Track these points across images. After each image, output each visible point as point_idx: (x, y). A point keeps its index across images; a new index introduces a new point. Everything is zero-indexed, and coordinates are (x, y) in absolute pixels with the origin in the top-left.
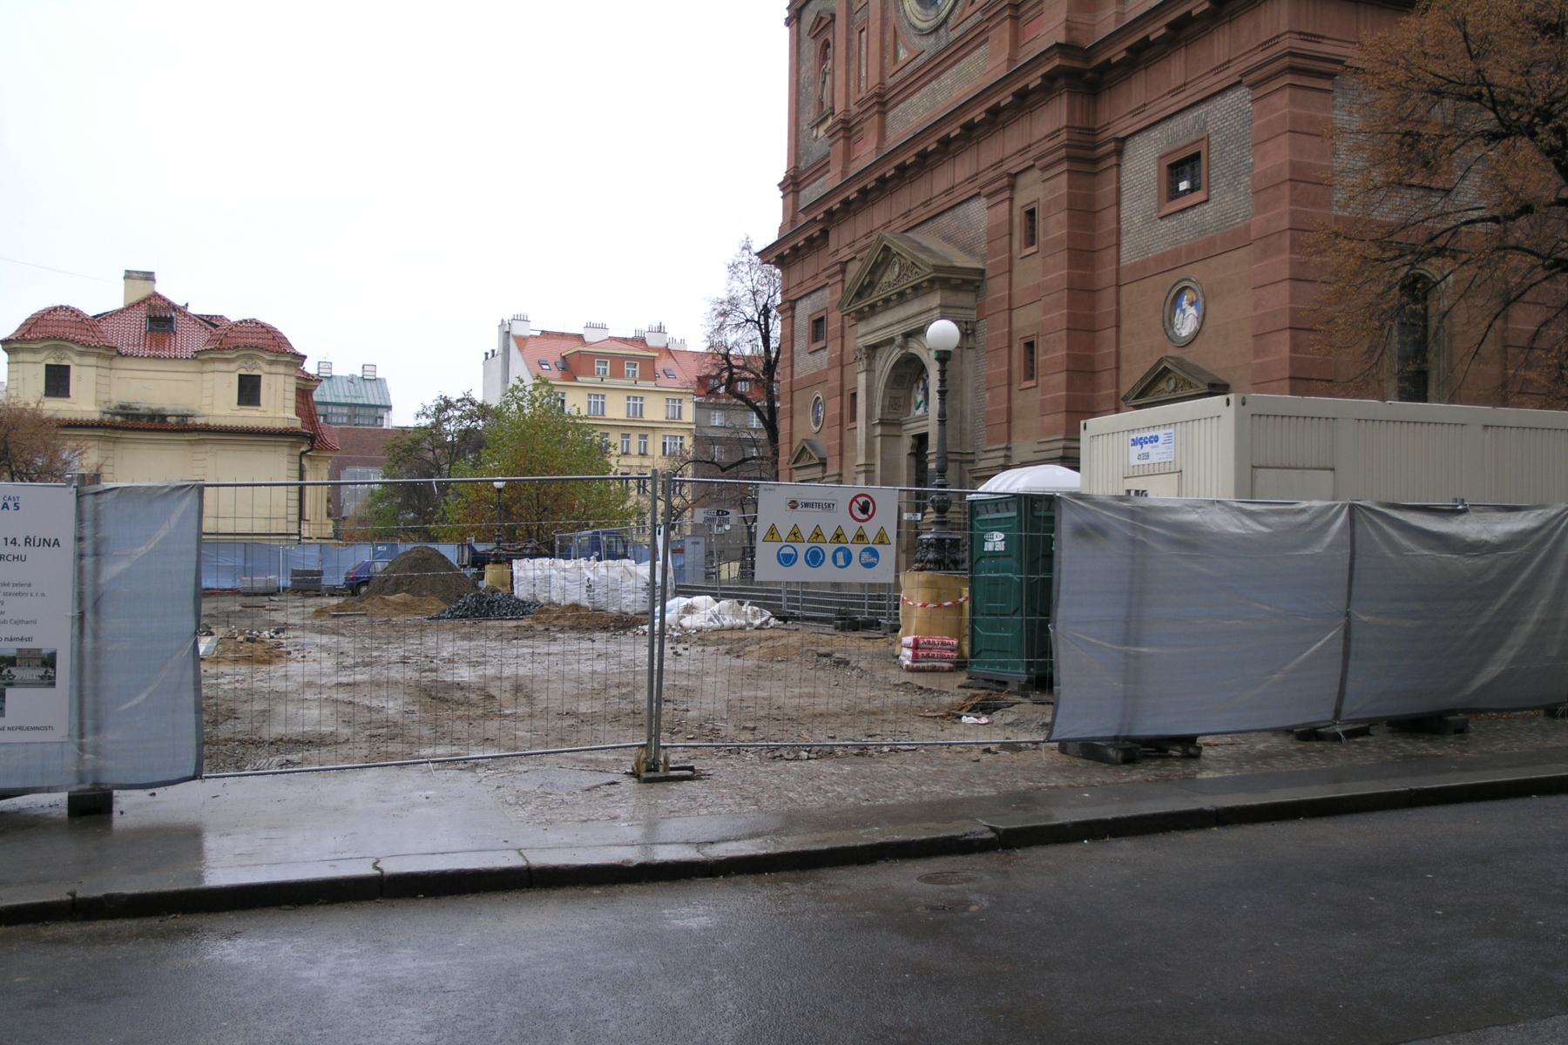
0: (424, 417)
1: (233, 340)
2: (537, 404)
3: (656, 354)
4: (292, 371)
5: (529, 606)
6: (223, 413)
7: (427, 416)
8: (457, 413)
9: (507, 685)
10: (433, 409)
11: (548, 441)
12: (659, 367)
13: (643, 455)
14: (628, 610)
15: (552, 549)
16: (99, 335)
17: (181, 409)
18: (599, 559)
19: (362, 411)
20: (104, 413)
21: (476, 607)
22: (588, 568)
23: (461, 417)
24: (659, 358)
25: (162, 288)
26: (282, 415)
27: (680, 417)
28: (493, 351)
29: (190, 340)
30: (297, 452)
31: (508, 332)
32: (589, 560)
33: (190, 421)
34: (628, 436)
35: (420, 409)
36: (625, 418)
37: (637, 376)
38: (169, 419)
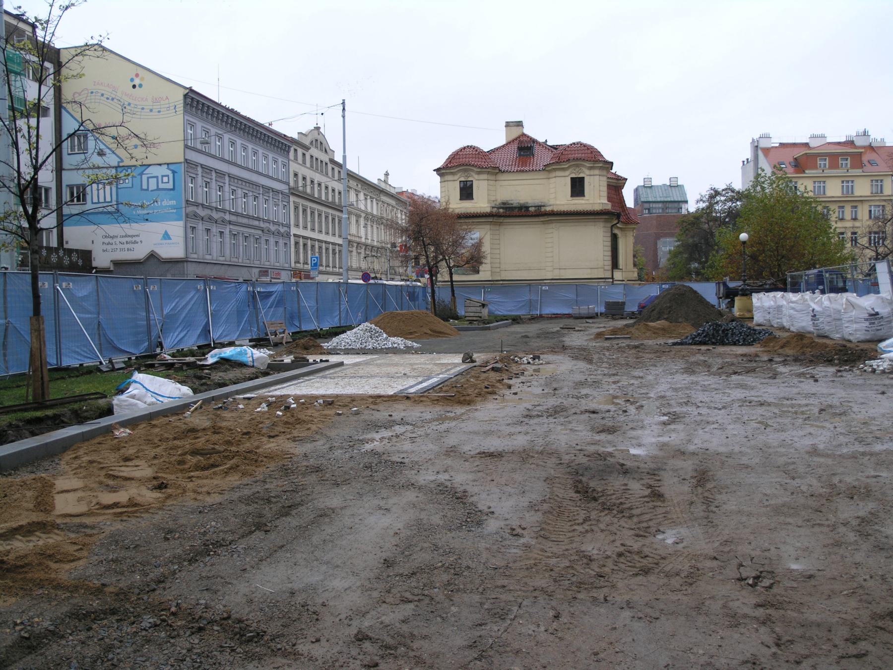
0: (701, 202)
1: (566, 156)
2: (774, 186)
3: (863, 150)
4: (605, 173)
5: (760, 333)
6: (562, 203)
7: (704, 202)
8: (723, 198)
9: (688, 466)
10: (707, 197)
11: (784, 210)
12: (865, 159)
13: (855, 219)
14: (851, 338)
15: (785, 284)
16: (488, 161)
17: (537, 202)
18: (823, 292)
19: (670, 205)
20: (493, 207)
21: (713, 334)
22: (812, 300)
23: (725, 200)
24: (865, 153)
25: (526, 131)
26: (599, 201)
27: (882, 192)
28: (748, 159)
29: (542, 158)
30: (609, 225)
31: (757, 146)
32: (814, 293)
33: (543, 209)
34: (843, 207)
35: (699, 197)
36: (840, 195)
37: (849, 166)
38: (530, 209)
